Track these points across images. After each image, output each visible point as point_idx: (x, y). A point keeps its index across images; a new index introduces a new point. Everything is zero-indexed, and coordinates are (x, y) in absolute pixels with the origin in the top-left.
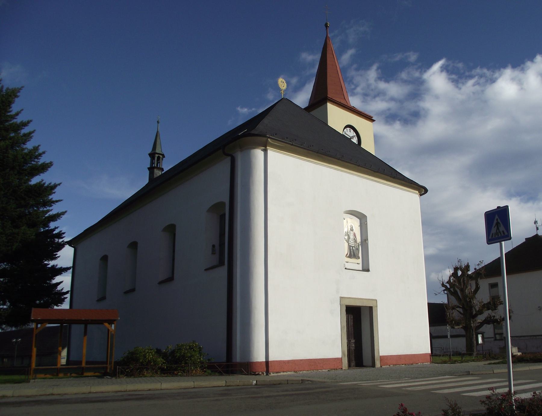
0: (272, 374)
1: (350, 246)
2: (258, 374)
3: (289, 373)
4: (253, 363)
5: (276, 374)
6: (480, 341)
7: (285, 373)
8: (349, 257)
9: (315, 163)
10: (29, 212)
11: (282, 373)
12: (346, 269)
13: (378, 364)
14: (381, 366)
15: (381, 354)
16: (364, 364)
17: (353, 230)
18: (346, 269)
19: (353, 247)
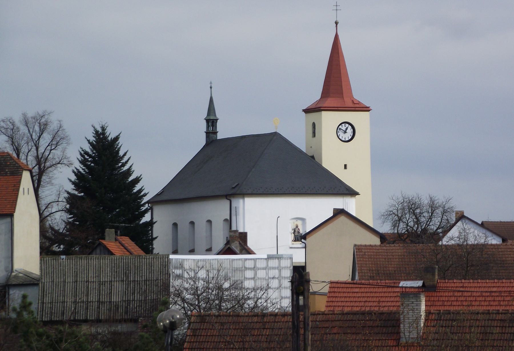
16: (304, 265)
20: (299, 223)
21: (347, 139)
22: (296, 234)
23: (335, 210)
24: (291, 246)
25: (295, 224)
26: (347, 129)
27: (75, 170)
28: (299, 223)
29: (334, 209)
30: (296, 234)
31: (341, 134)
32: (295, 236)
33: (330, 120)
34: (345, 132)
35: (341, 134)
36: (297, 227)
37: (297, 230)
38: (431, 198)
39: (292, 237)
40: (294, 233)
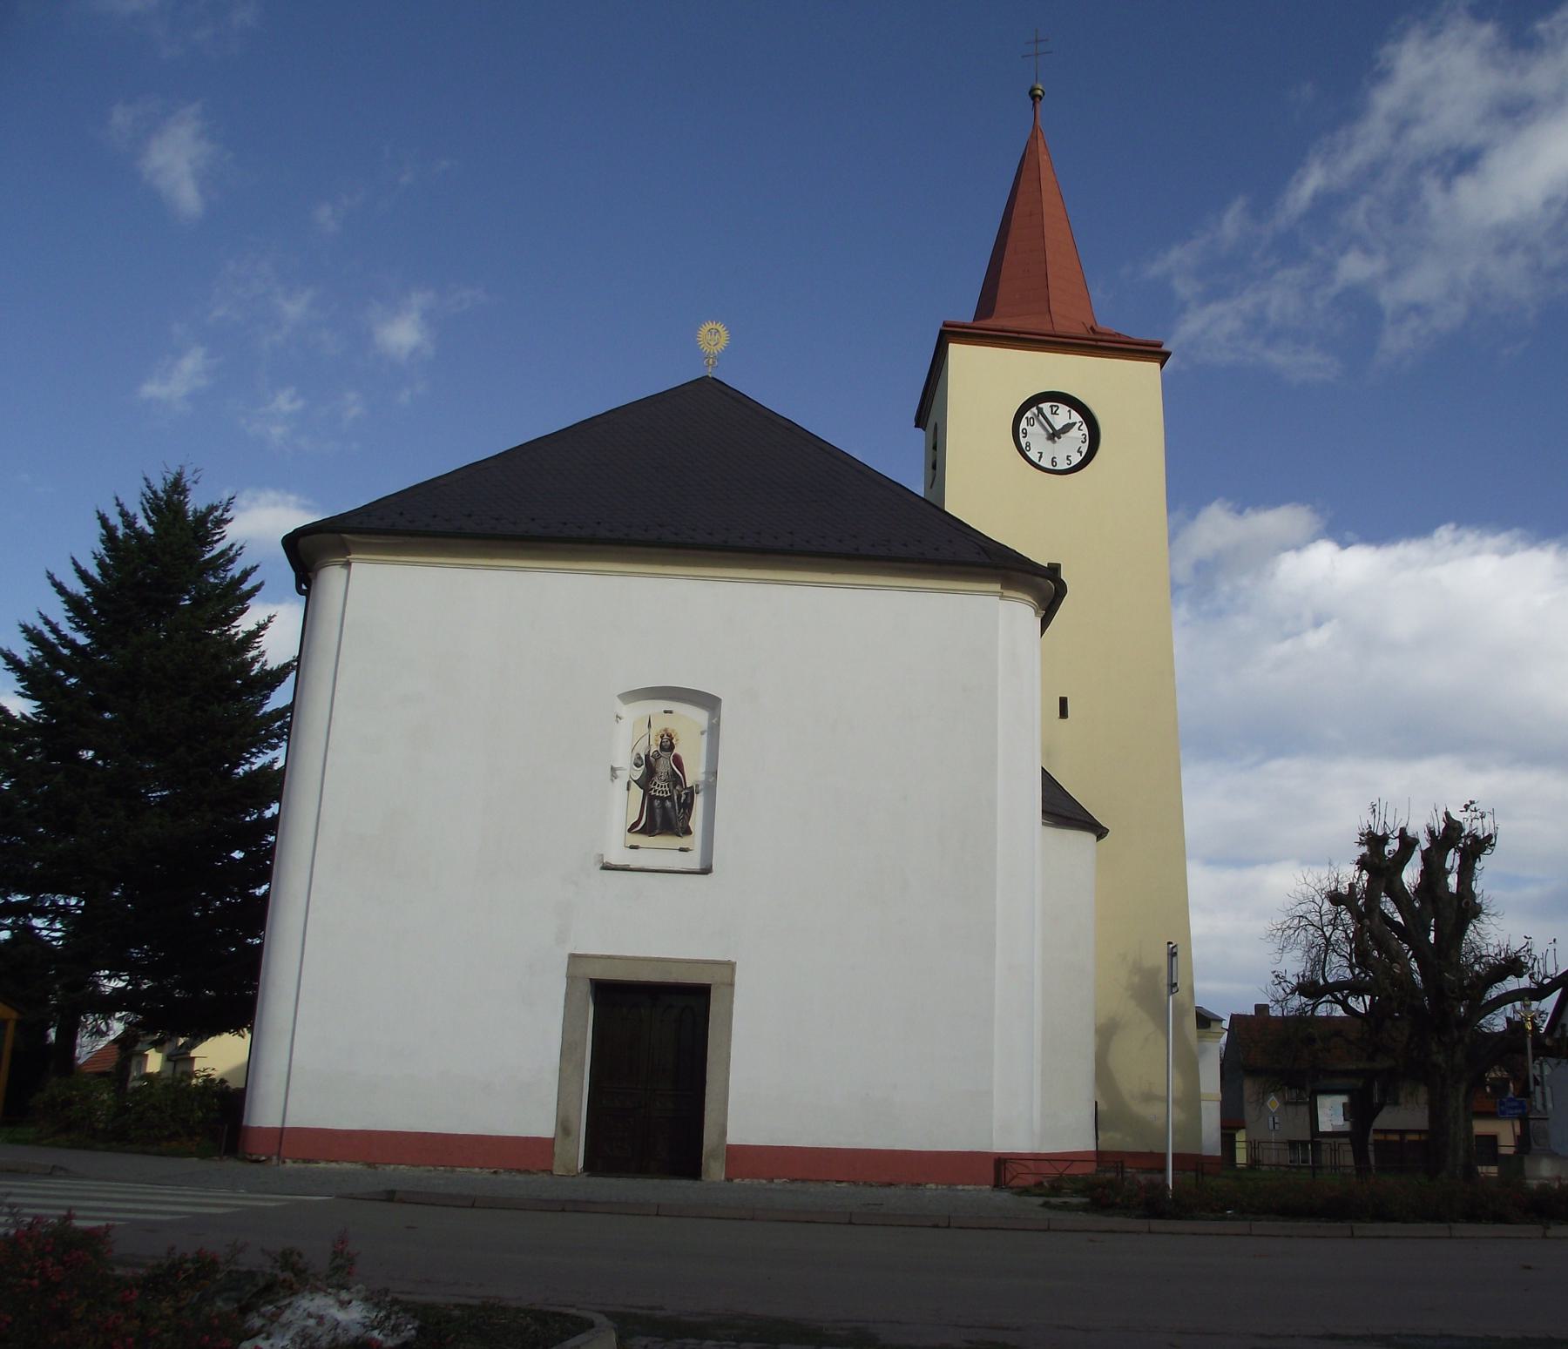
0: (289, 1164)
1: (652, 798)
2: (258, 1161)
3: (347, 1166)
4: (248, 1128)
5: (303, 1166)
6: (73, 680)
7: (334, 1165)
8: (643, 831)
9: (524, 569)
10: (54, 903)
11: (322, 1165)
12: (607, 867)
13: (715, 1170)
14: (729, 1179)
15: (733, 1138)
16: (242, 1085)
17: (672, 747)
18: (607, 867)
19: (663, 800)
20: (688, 723)
21: (1077, 459)
22: (660, 787)
23: (1054, 569)
24: (617, 856)
25: (657, 729)
26: (1068, 427)
27: (115, 520)
28: (688, 723)
29: (731, 966)
30: (660, 787)
31: (1035, 435)
32: (649, 798)
33: (987, 381)
34: (1054, 435)
35: (1035, 435)
36: (668, 744)
37: (664, 766)
38: (1490, 836)
39: (625, 804)
40: (645, 783)
